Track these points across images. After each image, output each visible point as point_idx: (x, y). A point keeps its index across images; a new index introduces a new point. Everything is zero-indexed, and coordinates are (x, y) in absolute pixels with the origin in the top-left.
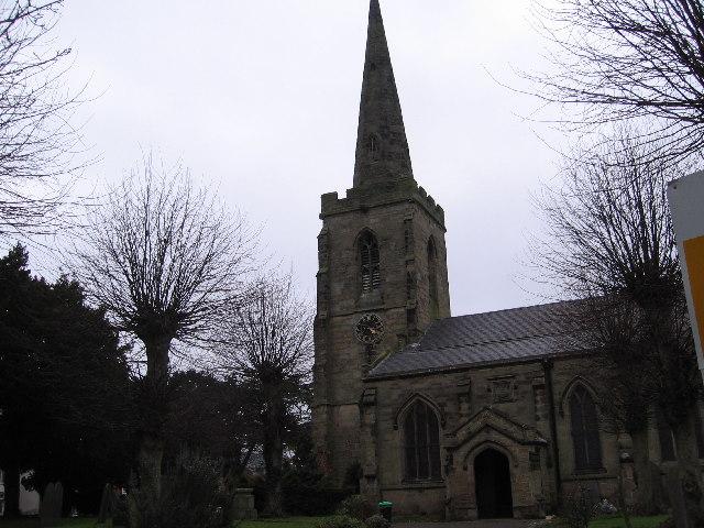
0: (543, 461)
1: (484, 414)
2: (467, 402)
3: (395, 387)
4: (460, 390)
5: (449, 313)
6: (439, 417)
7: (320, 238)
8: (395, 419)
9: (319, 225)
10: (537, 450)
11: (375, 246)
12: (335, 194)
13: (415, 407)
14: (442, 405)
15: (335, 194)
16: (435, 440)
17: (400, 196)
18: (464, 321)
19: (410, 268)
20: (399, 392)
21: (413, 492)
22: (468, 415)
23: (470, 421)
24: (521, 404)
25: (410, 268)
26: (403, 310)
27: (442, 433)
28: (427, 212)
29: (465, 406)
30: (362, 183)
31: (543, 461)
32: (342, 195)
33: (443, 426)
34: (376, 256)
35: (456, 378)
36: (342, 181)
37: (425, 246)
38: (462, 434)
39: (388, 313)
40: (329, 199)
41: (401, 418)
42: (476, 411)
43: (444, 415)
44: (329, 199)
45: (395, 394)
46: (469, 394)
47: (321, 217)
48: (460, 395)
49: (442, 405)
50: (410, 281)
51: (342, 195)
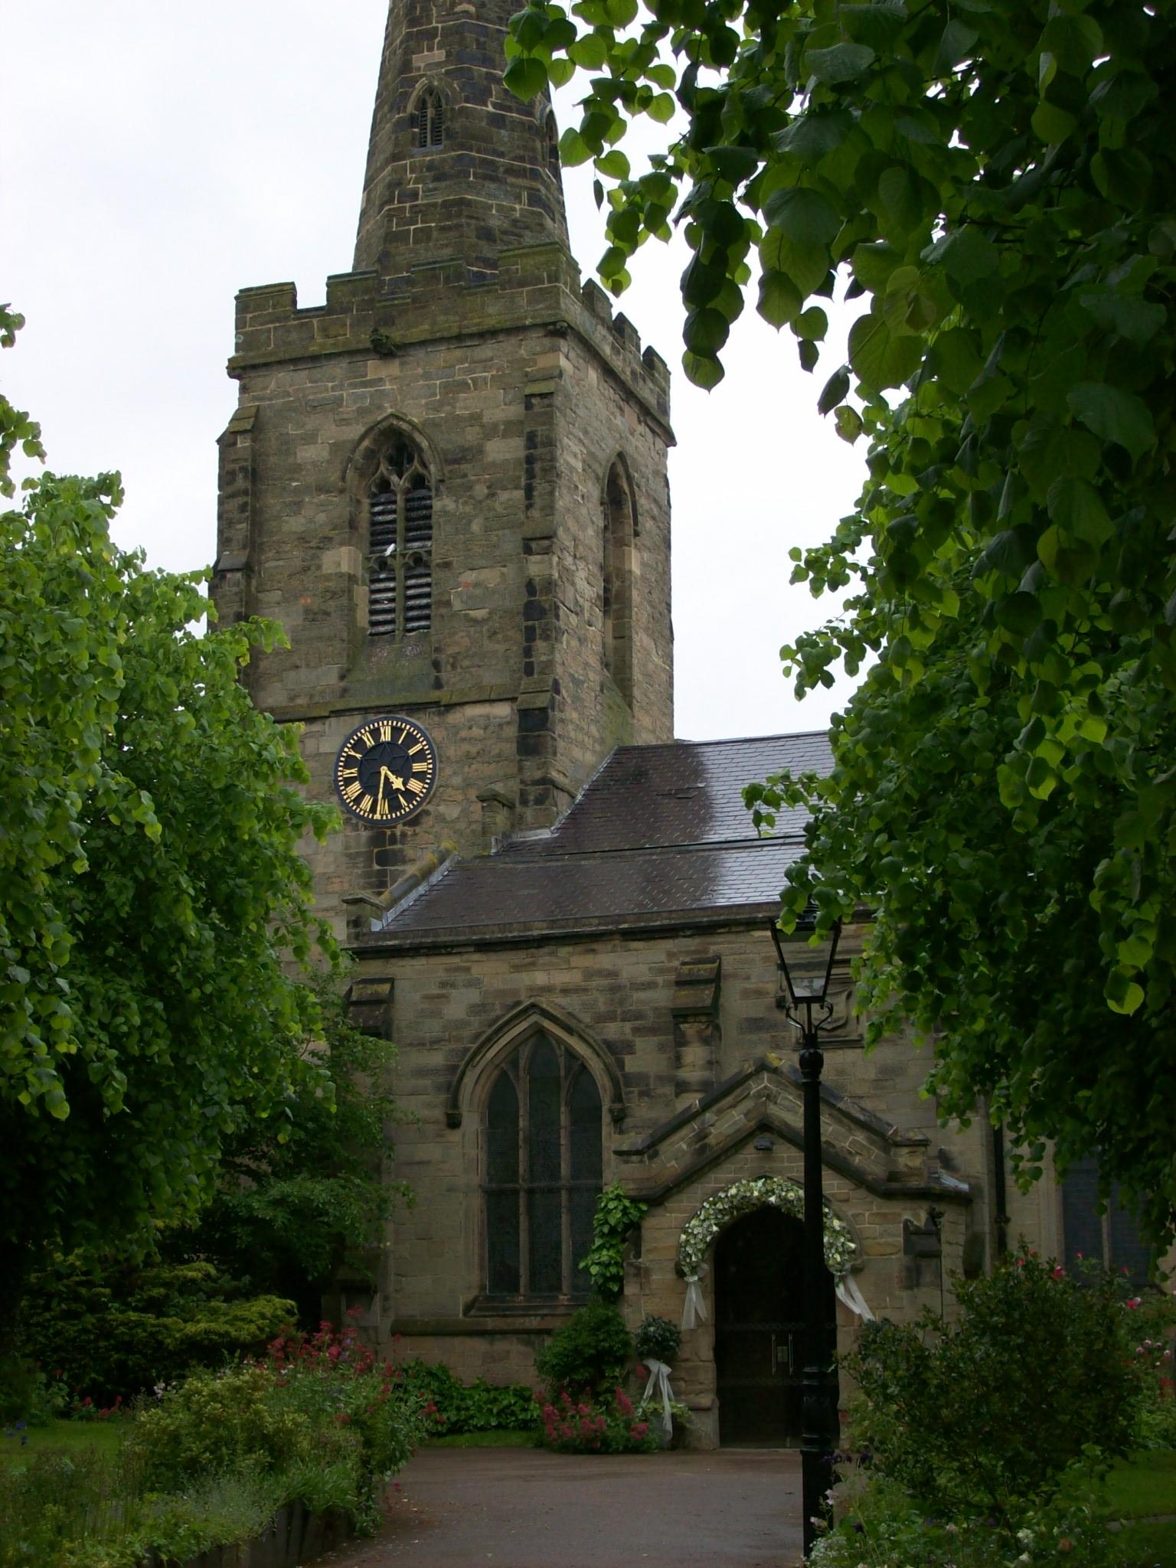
0: (952, 1254)
1: (754, 1087)
2: (706, 1041)
3: (461, 978)
4: (687, 998)
5: (671, 730)
6: (595, 1065)
7: (226, 443)
8: (453, 1091)
9: (225, 399)
10: (934, 1217)
11: (419, 482)
12: (287, 291)
13: (525, 1052)
14: (616, 1050)
15: (287, 291)
16: (590, 1164)
17: (525, 307)
18: (403, 253)
19: (535, 567)
20: (473, 996)
21: (501, 1345)
22: (705, 1086)
23: (705, 1107)
24: (883, 1054)
25: (535, 567)
26: (503, 710)
27: (611, 1141)
28: (608, 372)
29: (695, 1054)
30: (384, 258)
31: (952, 1254)
32: (312, 296)
33: (618, 1119)
34: (419, 522)
35: (671, 955)
36: (315, 243)
37: (592, 490)
38: (677, 1152)
39: (455, 717)
40: (263, 309)
41: (474, 1090)
42: (731, 1070)
43: (621, 1083)
44: (263, 309)
45: (458, 1005)
46: (711, 1014)
47: (236, 369)
48: (681, 1015)
49: (616, 1050)
50: (537, 610)
51: (312, 296)
